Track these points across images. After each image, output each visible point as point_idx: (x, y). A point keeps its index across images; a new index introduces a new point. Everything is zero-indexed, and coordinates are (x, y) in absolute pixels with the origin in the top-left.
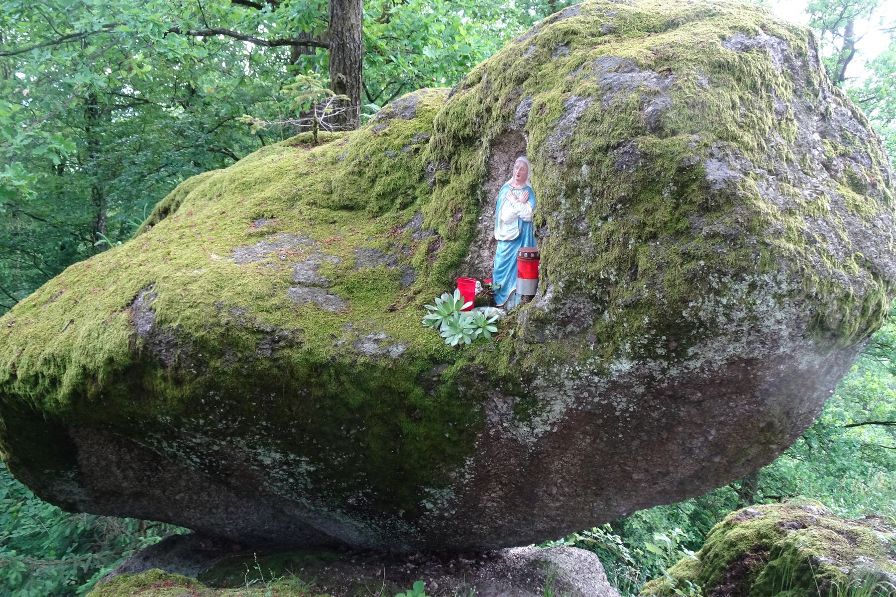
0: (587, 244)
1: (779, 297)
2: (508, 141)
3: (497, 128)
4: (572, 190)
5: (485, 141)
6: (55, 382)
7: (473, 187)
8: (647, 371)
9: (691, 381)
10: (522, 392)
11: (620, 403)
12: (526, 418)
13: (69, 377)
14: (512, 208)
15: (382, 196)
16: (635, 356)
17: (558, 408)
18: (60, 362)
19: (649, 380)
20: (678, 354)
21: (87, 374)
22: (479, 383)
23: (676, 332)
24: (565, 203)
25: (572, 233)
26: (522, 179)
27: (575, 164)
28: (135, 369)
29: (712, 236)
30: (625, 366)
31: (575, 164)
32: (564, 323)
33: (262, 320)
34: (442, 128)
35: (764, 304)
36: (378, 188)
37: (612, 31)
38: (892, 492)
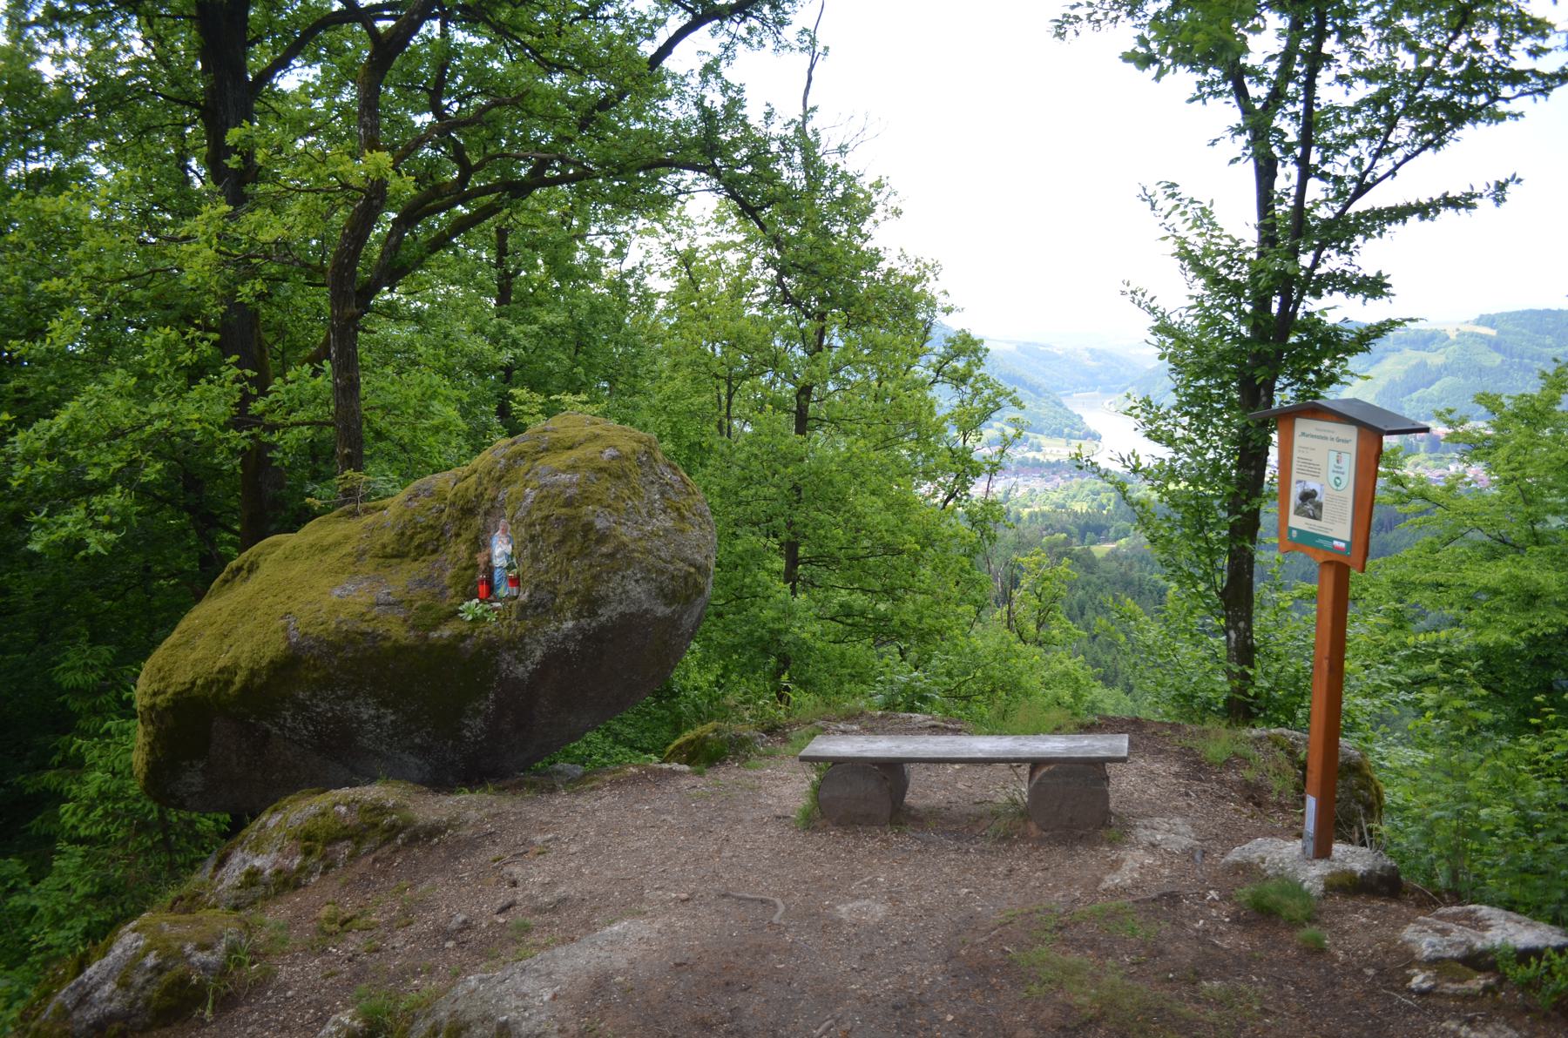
0: (543, 566)
1: (637, 581)
2: (494, 510)
3: (488, 505)
4: (532, 538)
5: (481, 511)
6: (229, 683)
7: (476, 538)
8: (55, 155)
9: (602, 627)
10: (516, 645)
11: (571, 646)
12: (521, 661)
13: (238, 680)
14: (500, 549)
15: (419, 546)
16: (574, 618)
17: (538, 653)
18: (229, 671)
19: (581, 630)
20: (593, 614)
21: (253, 673)
22: (493, 646)
23: (590, 604)
24: (530, 546)
25: (535, 558)
26: (504, 531)
27: (532, 525)
28: (289, 666)
29: (602, 555)
30: (570, 624)
31: (532, 525)
32: (536, 607)
33: (364, 627)
34: (453, 504)
35: (631, 585)
36: (416, 542)
37: (546, 450)
38: (1565, 819)
